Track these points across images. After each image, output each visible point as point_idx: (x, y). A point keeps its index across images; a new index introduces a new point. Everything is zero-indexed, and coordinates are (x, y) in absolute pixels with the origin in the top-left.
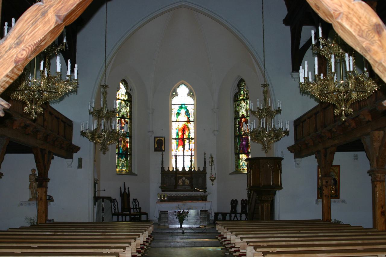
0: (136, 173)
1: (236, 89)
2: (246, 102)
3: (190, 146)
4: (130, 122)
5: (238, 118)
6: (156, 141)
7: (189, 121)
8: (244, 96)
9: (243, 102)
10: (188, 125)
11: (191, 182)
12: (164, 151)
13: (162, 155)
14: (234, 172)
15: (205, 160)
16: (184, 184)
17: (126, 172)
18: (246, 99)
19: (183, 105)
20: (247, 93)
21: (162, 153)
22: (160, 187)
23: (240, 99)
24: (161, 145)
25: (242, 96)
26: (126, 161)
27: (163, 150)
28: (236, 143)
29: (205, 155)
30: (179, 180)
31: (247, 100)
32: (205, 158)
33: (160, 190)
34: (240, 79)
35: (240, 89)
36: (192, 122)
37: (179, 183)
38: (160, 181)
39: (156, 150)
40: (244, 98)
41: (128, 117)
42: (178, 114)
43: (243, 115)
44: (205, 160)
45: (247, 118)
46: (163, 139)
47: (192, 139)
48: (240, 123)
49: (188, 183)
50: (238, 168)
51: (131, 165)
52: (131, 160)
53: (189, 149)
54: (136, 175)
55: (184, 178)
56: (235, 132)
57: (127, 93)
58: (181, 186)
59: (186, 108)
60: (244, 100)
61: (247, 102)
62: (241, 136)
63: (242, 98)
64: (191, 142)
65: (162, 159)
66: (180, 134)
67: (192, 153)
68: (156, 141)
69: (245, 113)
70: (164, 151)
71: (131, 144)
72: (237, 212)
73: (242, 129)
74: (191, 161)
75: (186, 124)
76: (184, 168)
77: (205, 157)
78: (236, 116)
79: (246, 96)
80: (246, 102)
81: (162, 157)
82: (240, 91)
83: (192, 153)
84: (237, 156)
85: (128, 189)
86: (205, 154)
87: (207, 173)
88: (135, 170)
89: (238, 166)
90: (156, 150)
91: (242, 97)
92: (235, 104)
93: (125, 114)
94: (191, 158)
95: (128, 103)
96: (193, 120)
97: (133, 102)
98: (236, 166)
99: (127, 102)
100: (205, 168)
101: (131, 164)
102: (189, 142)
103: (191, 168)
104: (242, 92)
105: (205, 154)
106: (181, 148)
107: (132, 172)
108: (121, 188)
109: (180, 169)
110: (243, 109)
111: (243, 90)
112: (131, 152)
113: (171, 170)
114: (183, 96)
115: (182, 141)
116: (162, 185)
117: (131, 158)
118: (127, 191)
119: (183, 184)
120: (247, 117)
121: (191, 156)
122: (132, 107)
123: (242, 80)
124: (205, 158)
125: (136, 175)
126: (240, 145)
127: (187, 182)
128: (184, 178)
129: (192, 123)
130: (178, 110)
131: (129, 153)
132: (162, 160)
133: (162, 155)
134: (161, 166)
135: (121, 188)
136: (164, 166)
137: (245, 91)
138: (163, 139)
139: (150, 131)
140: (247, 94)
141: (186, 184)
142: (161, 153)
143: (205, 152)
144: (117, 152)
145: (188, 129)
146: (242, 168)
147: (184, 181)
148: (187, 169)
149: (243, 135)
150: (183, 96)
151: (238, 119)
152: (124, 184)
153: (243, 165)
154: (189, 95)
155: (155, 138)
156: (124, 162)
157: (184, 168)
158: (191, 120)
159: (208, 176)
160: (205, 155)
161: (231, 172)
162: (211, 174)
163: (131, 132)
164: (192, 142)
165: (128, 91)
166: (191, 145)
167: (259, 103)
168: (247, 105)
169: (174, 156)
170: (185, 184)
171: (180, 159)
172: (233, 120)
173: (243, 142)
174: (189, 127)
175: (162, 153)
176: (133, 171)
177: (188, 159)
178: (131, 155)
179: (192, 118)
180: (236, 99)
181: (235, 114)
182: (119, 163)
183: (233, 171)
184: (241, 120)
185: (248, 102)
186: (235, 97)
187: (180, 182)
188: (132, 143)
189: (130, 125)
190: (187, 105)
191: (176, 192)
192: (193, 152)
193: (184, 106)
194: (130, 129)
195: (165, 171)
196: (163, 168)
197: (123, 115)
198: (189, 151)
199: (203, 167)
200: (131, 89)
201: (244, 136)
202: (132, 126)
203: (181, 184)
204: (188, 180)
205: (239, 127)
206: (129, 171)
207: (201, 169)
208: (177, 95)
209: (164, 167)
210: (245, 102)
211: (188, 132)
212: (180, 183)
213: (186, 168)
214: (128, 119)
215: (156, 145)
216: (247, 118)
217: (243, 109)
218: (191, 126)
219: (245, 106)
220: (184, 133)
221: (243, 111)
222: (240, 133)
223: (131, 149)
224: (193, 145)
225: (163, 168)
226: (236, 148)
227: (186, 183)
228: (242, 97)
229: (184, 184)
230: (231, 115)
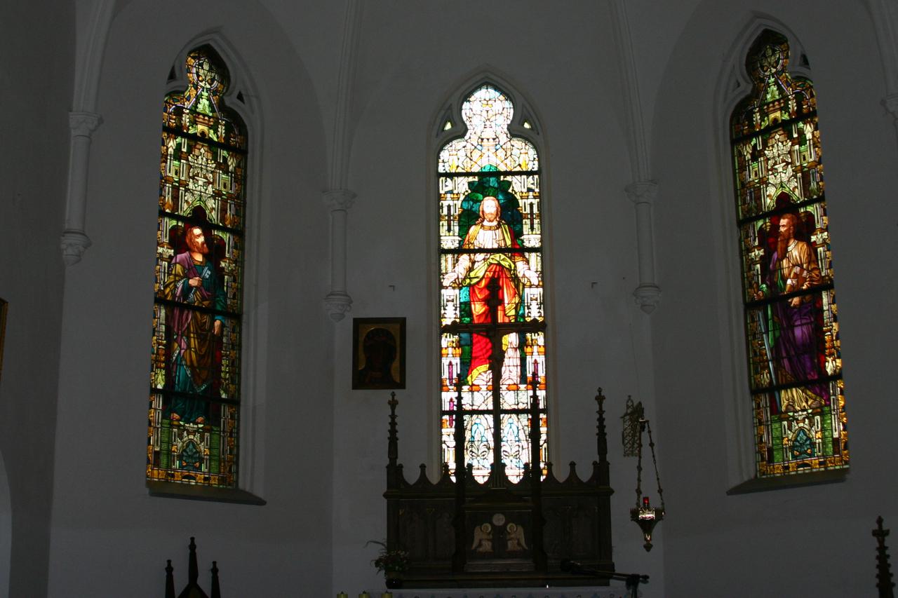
0: (259, 492)
1: (741, 80)
2: (795, 136)
3: (525, 359)
4: (235, 247)
5: (758, 218)
6: (362, 339)
7: (517, 250)
8: (781, 109)
9: (782, 138)
10: (515, 269)
11: (534, 537)
12: (402, 385)
13: (393, 404)
14: (750, 482)
15: (601, 427)
16: (500, 549)
17: (210, 485)
18: (795, 121)
19: (490, 174)
20: (799, 89)
21: (393, 395)
22: (377, 563)
23: (764, 124)
24: (384, 354)
25: (775, 111)
26: (210, 431)
27: (398, 380)
28: (751, 336)
29: (600, 404)
30: (477, 528)
31: (801, 125)
32: (601, 420)
33: (381, 577)
34: (759, 32)
35: (762, 80)
36: (533, 255)
37: (474, 546)
38: (383, 536)
39: (360, 381)
40: (786, 117)
41: (223, 219)
42: (470, 218)
43: (783, 199)
44: (601, 427)
45: (810, 209)
46: (398, 326)
47: (535, 326)
48: (771, 240)
49: (519, 544)
50: (771, 460)
51: (237, 456)
52: (234, 433)
53: (523, 378)
54: (261, 502)
55: (499, 520)
56: (747, 283)
57: (220, 106)
58: (484, 556)
59: (504, 188)
60: (786, 127)
61: (801, 133)
62: (777, 298)
63: (775, 120)
64: (532, 346)
65: (393, 424)
66: (478, 309)
67: (535, 397)
68: (362, 339)
69: (795, 189)
70: (402, 385)
71: (240, 350)
72: (67, 226)
73: (781, 269)
74: (534, 436)
75: (505, 264)
76: (498, 468)
77: (601, 412)
78: (750, 210)
79: (792, 105)
80: (795, 136)
81: (393, 416)
82: (759, 90)
83: (535, 397)
84: (764, 400)
85: (215, 571)
86: (600, 399)
87: (612, 492)
88: (251, 478)
89: (770, 451)
90: (360, 381)
91: (772, 116)
92: (741, 155)
93: (211, 203)
94: (535, 425)
95: (225, 159)
96: (538, 245)
97: (249, 156)
98: (760, 452)
99: (225, 153)
100: (602, 469)
101: (238, 446)
102: (523, 344)
103: (531, 471)
104: (773, 93)
105: (600, 399)
106: (481, 375)
107: (241, 485)
108: (169, 569)
109: (481, 475)
110: (785, 168)
111: (776, 83)
112: (239, 390)
113: (434, 478)
114: (488, 131)
115: (483, 337)
116: (389, 549)
117: (235, 417)
118: (204, 582)
119: (493, 547)
120: (804, 204)
121: (534, 410)
122: (245, 178)
123: (769, 40)
124: (601, 420)
125: (261, 502)
126: (775, 349)
127: (517, 536)
128: (499, 520)
129: (534, 259)
130: (467, 198)
131: (224, 396)
132: (393, 432)
133: (393, 404)
134: (387, 461)
135: (169, 569)
136: (399, 462)
137: (789, 85)
138: (394, 329)
139: (332, 294)
140: (799, 99)
141: (511, 545)
142: (386, 394)
143: (600, 390)
144: (160, 387)
145: (517, 287)
146: (794, 457)
147: (499, 533)
148: (514, 474)
149: (792, 295)
150: (488, 131)
151: (760, 223)
152: (193, 547)
153: (802, 445)
154: (514, 131)
155: (357, 322)
156: (196, 438)
157: (498, 468)
158: (527, 244)
159: (620, 506)
160: (600, 404)
161: (735, 481)
162: (639, 492)
163: (238, 294)
164: (535, 348)
165: (231, 101)
166: (529, 360)
167: (774, 368)
168: (803, 148)
169: (450, 413)
170: (506, 545)
171: (480, 428)
172: (735, 228)
173: (792, 327)
174: (520, 275)
175: (393, 395)
176: (244, 484)
177: (516, 428)
178: (234, 402)
179: (532, 237)
180: (743, 127)
181: (744, 202)
182: (170, 443)
183: (746, 479)
184: (776, 226)
185: (808, 131)
186: (738, 123)
187: (482, 538)
188: (244, 344)
189: (235, 262)
190: (509, 178)
191: (460, 587)
192: (541, 394)
193: (493, 181)
194: (235, 281)
195: (406, 483)
196: (394, 471)
197: (199, 207)
198: (523, 387)
199: (595, 463)
200: (243, 92)
201: (796, 300)
202: (243, 268)
203: (487, 546)
204: (520, 530)
205: (764, 261)
206: (222, 481)
207: (585, 473)
208: (460, 131)
209: (401, 466)
210: (790, 137)
211: (517, 300)
212: (480, 545)
213: (508, 472)
214: (224, 229)
215: (362, 356)
216: (810, 209)
217: (785, 168)
218: (529, 269)
219: (790, 152)
220: (493, 300)
221: (785, 179)
222: (773, 286)
223: (239, 374)
224: (541, 359)
225: (394, 471)
226: (756, 364)
227: (509, 543)
228: (772, 116)
229: (500, 549)
230: (724, 210)
